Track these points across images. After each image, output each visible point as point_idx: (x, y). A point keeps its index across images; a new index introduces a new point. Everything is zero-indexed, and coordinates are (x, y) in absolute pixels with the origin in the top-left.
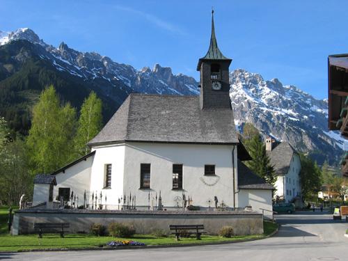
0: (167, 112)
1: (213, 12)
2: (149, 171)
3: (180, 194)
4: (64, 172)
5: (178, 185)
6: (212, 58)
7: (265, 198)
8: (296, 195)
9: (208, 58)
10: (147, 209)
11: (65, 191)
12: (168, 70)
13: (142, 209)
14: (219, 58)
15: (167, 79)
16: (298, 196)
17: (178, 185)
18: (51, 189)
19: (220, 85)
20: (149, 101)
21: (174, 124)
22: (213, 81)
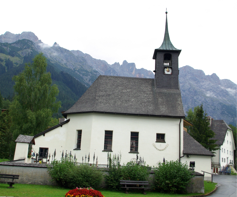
0: (128, 90)
1: (166, 13)
2: (132, 147)
3: (134, 156)
4: (44, 136)
5: (134, 149)
6: (165, 49)
7: (9, 159)
8: (229, 162)
9: (161, 49)
10: (231, 152)
11: (44, 150)
12: (133, 65)
13: (102, 167)
14: (171, 49)
15: (132, 71)
16: (230, 163)
17: (134, 149)
18: (30, 149)
19: (171, 70)
20: (114, 81)
21: (133, 100)
22: (166, 67)
